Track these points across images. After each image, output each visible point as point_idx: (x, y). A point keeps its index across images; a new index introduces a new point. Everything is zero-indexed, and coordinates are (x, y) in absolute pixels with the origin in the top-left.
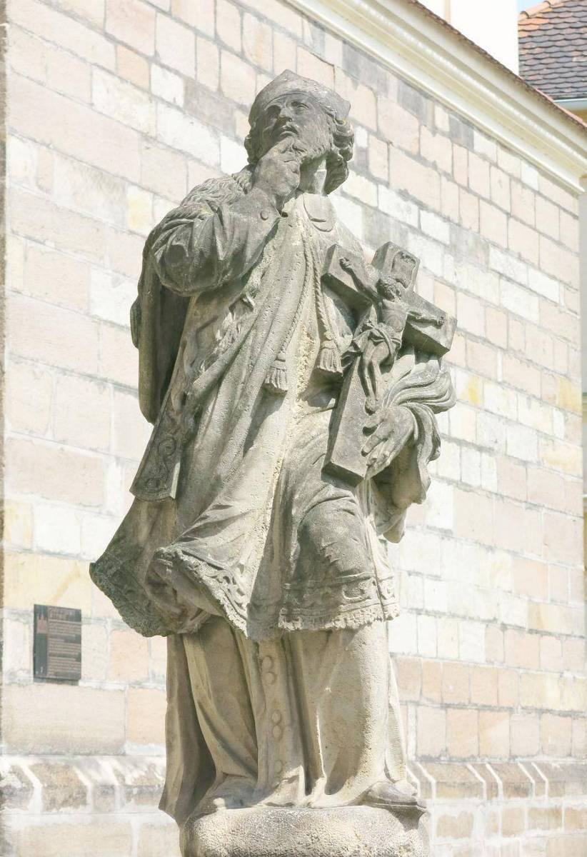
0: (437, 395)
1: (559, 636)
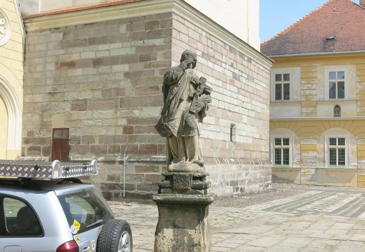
1: (265, 140)
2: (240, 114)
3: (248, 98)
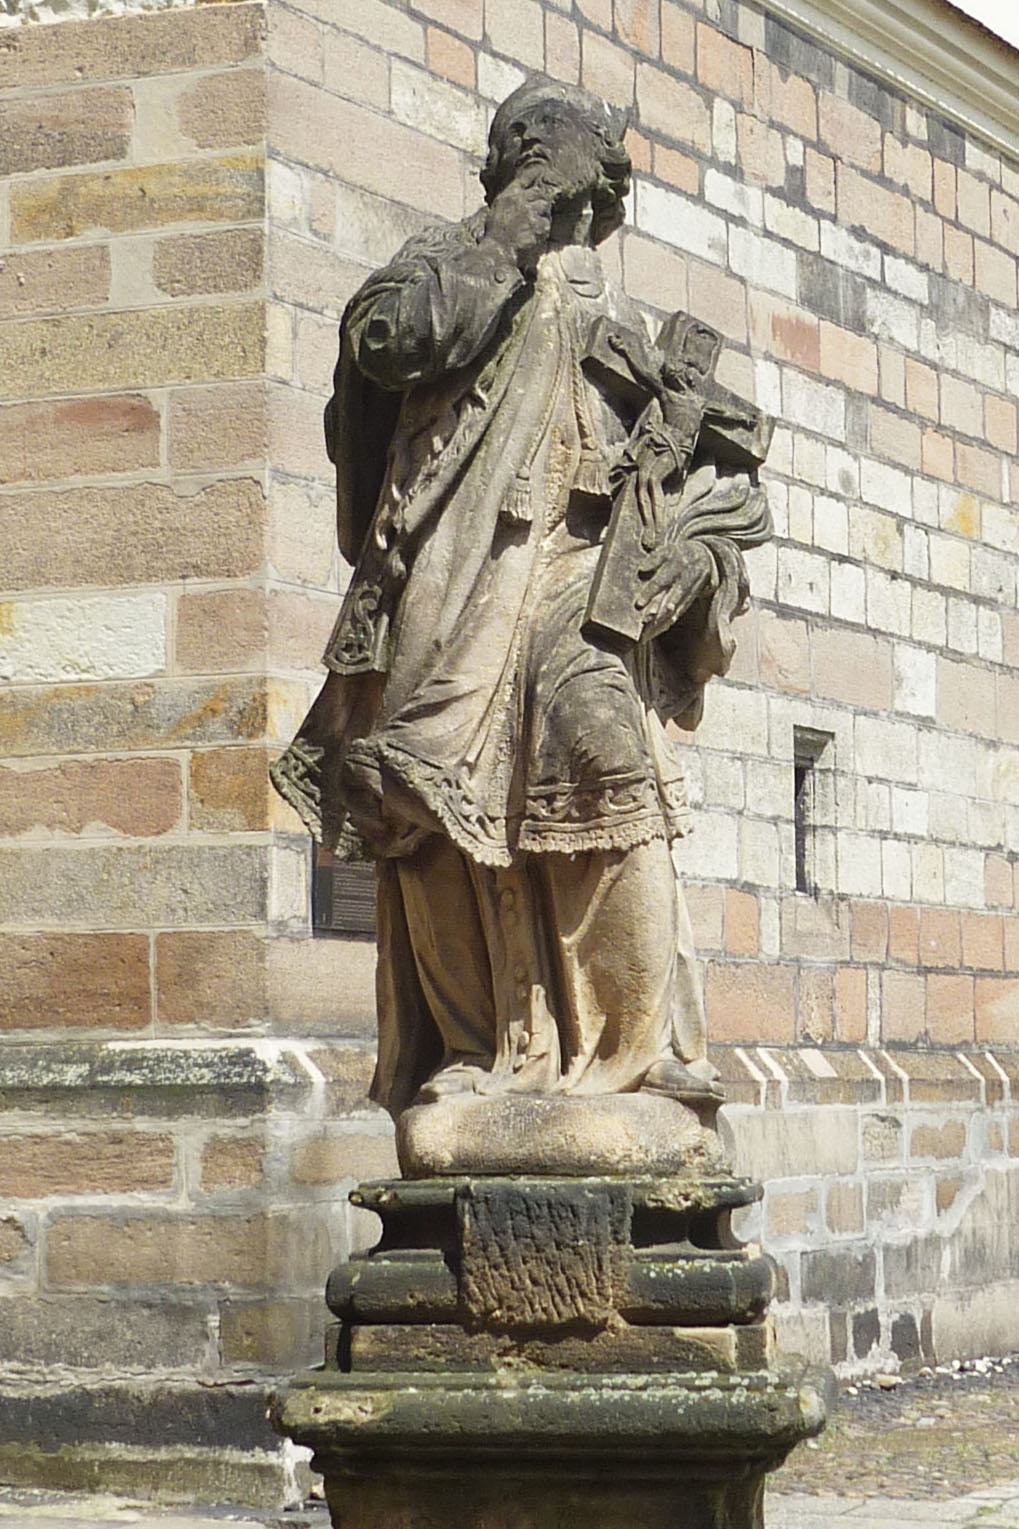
0: (745, 523)
2: (876, 632)
3: (944, 491)
